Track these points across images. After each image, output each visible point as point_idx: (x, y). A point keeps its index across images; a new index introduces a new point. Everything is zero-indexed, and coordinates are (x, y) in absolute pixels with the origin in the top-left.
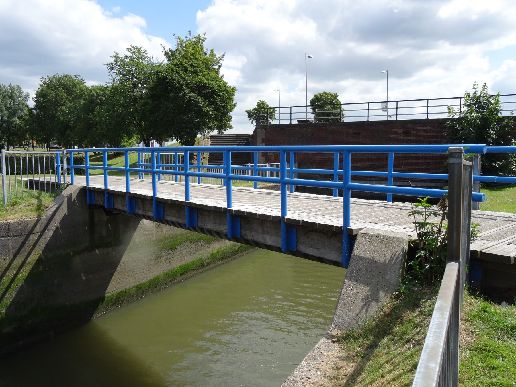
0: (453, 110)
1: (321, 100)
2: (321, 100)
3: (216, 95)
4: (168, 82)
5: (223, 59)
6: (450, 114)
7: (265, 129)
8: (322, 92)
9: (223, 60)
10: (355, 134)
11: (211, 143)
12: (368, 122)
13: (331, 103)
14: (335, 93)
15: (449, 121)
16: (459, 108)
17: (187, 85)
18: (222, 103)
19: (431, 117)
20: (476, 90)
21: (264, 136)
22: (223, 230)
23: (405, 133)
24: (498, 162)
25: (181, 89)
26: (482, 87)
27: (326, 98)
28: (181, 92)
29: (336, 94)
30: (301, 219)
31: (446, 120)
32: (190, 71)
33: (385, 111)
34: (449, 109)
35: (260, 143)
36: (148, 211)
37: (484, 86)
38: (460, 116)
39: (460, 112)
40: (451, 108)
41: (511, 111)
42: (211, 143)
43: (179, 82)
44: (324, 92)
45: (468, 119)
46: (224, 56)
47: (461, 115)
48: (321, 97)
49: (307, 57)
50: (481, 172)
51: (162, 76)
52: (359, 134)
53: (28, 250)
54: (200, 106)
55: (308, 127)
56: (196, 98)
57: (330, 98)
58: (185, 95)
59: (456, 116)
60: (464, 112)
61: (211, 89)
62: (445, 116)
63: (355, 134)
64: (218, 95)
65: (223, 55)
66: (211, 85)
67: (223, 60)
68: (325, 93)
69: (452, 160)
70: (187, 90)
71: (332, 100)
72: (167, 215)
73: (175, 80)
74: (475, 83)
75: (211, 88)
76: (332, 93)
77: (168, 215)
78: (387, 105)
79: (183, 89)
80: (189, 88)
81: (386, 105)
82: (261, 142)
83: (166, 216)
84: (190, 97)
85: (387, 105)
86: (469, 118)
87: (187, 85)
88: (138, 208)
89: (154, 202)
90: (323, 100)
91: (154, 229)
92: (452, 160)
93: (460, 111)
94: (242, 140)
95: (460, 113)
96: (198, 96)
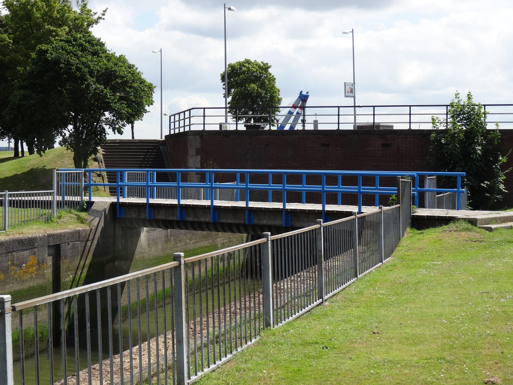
0: (439, 120)
1: (240, 74)
2: (240, 74)
3: (128, 87)
4: (62, 68)
5: (103, 17)
6: (435, 125)
7: (201, 137)
8: (242, 60)
9: (104, 19)
10: (323, 145)
11: (104, 153)
12: (338, 130)
13: (257, 79)
14: (265, 62)
15: (434, 133)
16: (446, 118)
17: (91, 73)
18: (135, 97)
19: (414, 127)
20: (459, 99)
21: (198, 146)
22: (277, 223)
23: (383, 145)
24: (486, 182)
25: (83, 78)
26: (467, 96)
27: (249, 70)
28: (83, 84)
29: (267, 64)
30: (335, 210)
31: (429, 132)
32: (89, 51)
33: (351, 97)
34: (433, 119)
35: (193, 155)
36: (200, 218)
37: (468, 95)
38: (447, 127)
39: (447, 123)
40: (435, 118)
41: (496, 123)
42: (104, 153)
43: (78, 69)
44: (246, 60)
45: (451, 133)
46: (106, 14)
47: (448, 126)
48: (241, 69)
49: (227, 10)
50: (468, 193)
51: (52, 59)
52: (327, 145)
53: (86, 255)
54: (109, 103)
55: (261, 135)
56: (102, 91)
57: (256, 71)
58: (88, 85)
59: (442, 127)
60: (450, 123)
61: (121, 79)
62: (429, 127)
63: (323, 145)
64: (131, 87)
65: (105, 11)
66: (122, 73)
67: (104, 19)
68: (248, 61)
69: (398, 179)
70: (91, 80)
71: (260, 73)
72: (222, 219)
73: (73, 65)
74: (457, 92)
75: (122, 77)
76: (260, 63)
77: (223, 219)
78: (353, 87)
79: (86, 79)
80: (93, 77)
81: (351, 87)
82: (195, 154)
83: (221, 219)
84: (95, 89)
85: (353, 87)
86: (452, 132)
87: (91, 73)
88: (188, 216)
89: (212, 210)
90: (243, 73)
91: (147, 247)
92: (398, 179)
93: (447, 121)
94: (151, 149)
95: (447, 124)
96: (105, 88)
